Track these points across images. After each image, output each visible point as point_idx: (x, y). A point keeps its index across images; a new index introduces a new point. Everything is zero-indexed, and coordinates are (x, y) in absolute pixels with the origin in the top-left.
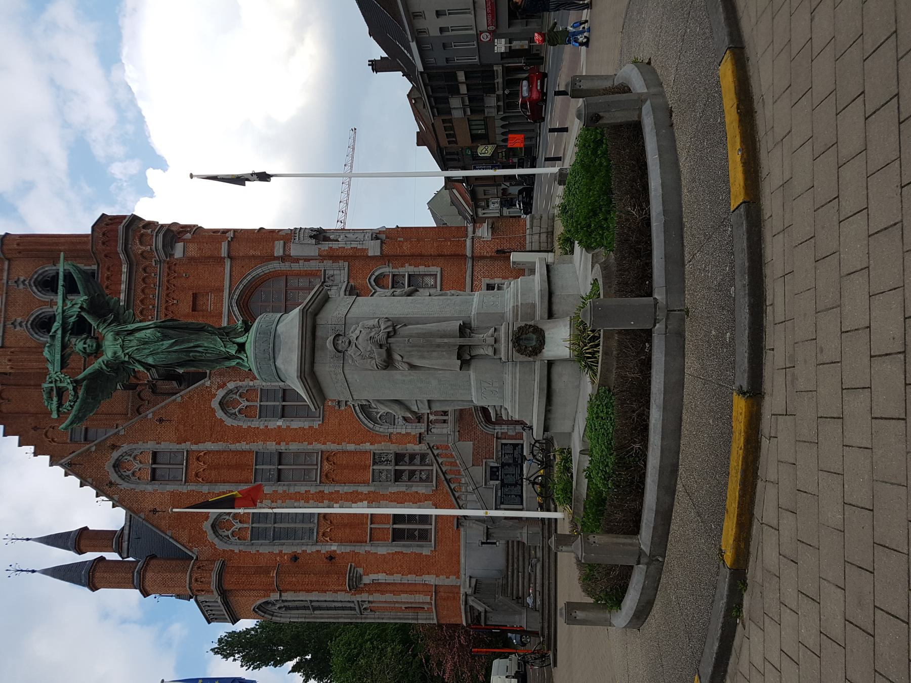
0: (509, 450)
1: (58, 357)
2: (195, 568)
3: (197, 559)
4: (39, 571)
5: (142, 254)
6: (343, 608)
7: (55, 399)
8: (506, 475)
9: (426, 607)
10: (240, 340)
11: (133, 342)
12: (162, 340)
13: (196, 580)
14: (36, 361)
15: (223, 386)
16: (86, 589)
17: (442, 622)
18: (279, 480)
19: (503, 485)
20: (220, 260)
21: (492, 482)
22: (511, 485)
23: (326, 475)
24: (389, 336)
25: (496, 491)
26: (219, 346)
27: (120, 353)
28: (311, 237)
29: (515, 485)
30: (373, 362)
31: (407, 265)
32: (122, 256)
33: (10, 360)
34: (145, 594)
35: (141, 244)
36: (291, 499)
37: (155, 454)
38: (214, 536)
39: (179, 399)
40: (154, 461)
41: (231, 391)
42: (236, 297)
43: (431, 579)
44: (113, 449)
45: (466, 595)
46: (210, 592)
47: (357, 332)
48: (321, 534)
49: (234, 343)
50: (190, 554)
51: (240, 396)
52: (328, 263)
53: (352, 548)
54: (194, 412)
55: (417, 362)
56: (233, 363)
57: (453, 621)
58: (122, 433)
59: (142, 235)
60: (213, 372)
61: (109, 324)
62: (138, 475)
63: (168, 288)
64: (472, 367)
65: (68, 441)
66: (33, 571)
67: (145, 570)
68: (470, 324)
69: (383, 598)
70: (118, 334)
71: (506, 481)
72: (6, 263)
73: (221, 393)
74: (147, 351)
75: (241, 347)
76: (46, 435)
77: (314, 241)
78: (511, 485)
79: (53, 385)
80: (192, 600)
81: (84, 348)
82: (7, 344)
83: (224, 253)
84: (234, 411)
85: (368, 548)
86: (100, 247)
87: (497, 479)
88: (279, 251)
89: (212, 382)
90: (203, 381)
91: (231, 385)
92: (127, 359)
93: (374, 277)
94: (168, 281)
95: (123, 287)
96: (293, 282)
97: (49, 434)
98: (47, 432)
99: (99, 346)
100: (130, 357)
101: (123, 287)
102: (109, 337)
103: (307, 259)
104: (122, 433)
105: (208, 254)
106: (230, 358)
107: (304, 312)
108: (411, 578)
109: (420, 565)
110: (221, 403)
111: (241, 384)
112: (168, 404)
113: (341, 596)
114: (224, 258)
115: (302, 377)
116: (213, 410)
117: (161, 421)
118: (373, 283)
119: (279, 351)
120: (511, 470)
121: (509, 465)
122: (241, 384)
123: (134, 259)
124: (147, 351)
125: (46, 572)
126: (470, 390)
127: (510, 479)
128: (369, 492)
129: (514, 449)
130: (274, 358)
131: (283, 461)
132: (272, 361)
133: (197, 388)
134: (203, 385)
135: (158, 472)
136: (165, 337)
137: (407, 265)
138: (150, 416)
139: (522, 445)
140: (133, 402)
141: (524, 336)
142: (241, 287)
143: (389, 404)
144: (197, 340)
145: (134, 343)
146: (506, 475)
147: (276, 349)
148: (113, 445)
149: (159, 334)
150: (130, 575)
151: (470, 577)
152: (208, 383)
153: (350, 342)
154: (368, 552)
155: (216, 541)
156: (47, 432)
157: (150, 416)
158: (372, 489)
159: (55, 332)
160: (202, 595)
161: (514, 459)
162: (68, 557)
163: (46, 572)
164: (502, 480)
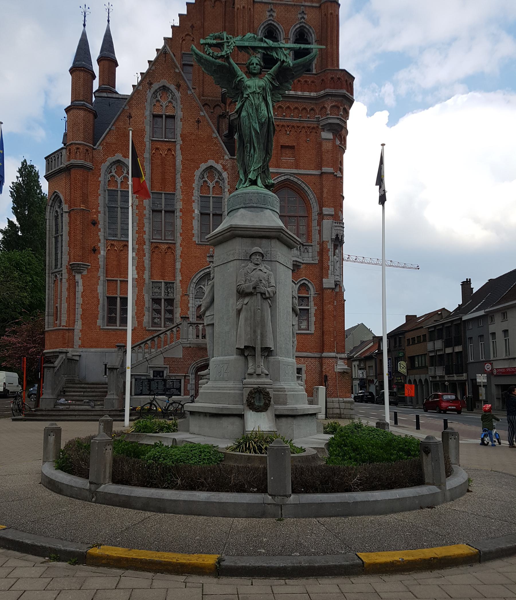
0: (176, 385)
1: (246, 44)
2: (87, 148)
3: (94, 149)
5: (324, 107)
6: (56, 260)
7: (215, 42)
8: (157, 383)
10: (259, 181)
11: (257, 100)
12: (259, 123)
13: (78, 148)
16: (71, 65)
17: (46, 335)
19: (150, 380)
20: (319, 166)
22: (150, 387)
23: (157, 247)
24: (262, 294)
25: (145, 375)
27: (249, 91)
28: (337, 235)
29: (150, 390)
32: (322, 92)
35: (332, 107)
37: (173, 117)
40: (167, 117)
41: (220, 174)
42: (292, 178)
43: (78, 326)
44: (177, 85)
45: (67, 353)
46: (69, 158)
47: (265, 270)
49: (257, 177)
50: (98, 144)
51: (217, 182)
52: (317, 248)
53: (102, 267)
54: (204, 147)
55: (242, 315)
57: (47, 342)
58: (189, 92)
60: (235, 161)
62: (157, 104)
63: (298, 127)
64: (239, 357)
65: (183, 52)
66: (84, 25)
67: (85, 110)
70: (264, 89)
72: (317, 5)
73: (219, 167)
75: (254, 183)
77: (334, 237)
78: (150, 387)
79: (225, 40)
80: (63, 145)
81: (253, 64)
82: (256, 5)
83: (325, 169)
84: (205, 177)
85: (102, 278)
86: (330, 76)
87: (154, 376)
88: (326, 211)
89: (227, 160)
90: (228, 153)
91: (225, 175)
92: (245, 96)
93: (307, 283)
94: (304, 127)
95: (300, 93)
97: (188, 38)
98: (190, 35)
99: (255, 75)
100: (247, 98)
101: (300, 93)
102: (262, 83)
103: (320, 232)
104: (189, 92)
109: (89, 318)
110: (211, 167)
111: (226, 182)
112: (211, 127)
114: (321, 170)
115: (232, 228)
117: (198, 122)
118: (302, 282)
119: (251, 211)
120: (161, 387)
121: (165, 385)
122: (226, 182)
123: (322, 100)
124: (251, 111)
125: (84, 35)
126: (222, 355)
127: (154, 385)
128: (144, 279)
129: (177, 389)
132: (244, 206)
133: (223, 149)
134: (226, 153)
135: (159, 120)
136: (261, 125)
139: (180, 395)
140: (212, 100)
141: (262, 396)
142: (299, 182)
143: (211, 294)
145: (257, 102)
146: (157, 383)
147: (252, 209)
148: (180, 85)
149: (263, 120)
150: (81, 98)
151: (80, 356)
152: (226, 157)
153: (257, 265)
155: (107, 164)
156: (190, 35)
158: (147, 281)
159: (265, 42)
160: (66, 153)
161: (170, 389)
163: (84, 35)
164: (153, 380)
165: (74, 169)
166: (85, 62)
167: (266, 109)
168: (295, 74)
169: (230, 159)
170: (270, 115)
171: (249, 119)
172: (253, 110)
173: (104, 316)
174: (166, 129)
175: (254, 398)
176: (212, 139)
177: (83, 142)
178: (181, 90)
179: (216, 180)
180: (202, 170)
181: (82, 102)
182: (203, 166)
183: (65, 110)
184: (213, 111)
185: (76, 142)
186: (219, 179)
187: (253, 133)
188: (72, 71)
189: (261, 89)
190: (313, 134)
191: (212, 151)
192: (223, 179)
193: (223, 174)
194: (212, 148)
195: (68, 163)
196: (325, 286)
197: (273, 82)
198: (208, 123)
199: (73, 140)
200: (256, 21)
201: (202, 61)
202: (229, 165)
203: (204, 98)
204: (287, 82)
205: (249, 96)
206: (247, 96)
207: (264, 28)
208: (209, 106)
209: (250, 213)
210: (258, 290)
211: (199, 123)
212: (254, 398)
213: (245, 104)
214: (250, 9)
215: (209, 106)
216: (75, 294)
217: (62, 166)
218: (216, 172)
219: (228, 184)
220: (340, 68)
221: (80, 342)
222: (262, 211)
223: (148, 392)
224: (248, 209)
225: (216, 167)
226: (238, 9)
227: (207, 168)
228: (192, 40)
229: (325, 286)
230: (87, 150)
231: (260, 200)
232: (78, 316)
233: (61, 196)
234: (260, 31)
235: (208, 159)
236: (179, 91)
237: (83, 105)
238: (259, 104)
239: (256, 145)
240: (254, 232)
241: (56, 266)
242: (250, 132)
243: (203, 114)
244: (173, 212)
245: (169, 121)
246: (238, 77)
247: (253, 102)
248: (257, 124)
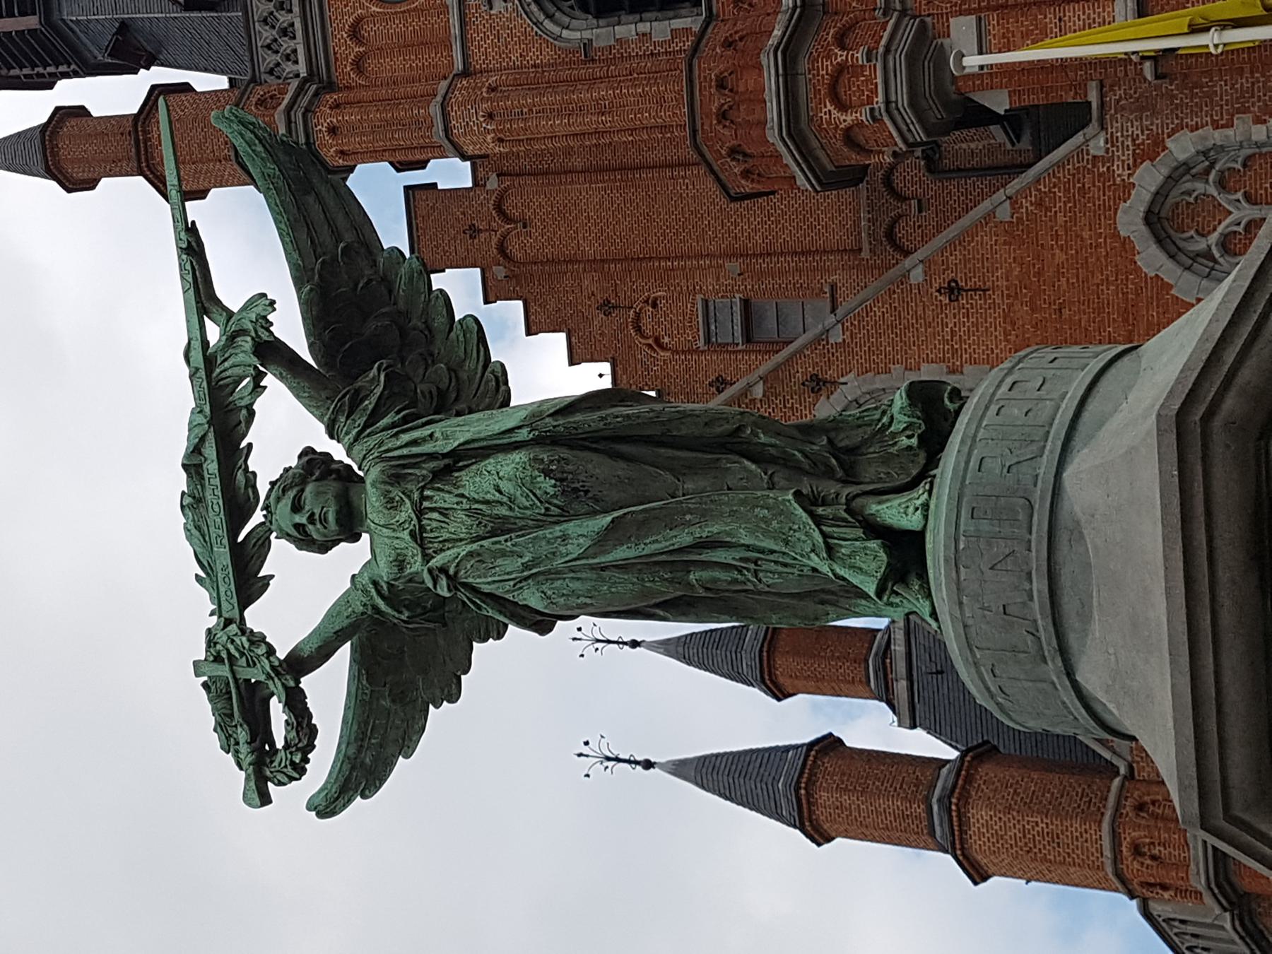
2: (1128, 808)
4: (663, 766)
12: (566, 515)
13: (1137, 850)
14: (560, 114)
15: (1151, 150)
27: (416, 565)
33: (490, 116)
34: (977, 874)
39: (1004, 213)
41: (1184, 168)
44: (816, 391)
49: (875, 529)
50: (1107, 755)
51: (1222, 184)
54: (1060, 256)
58: (837, 337)
60: (1111, 98)
65: (701, 344)
66: (648, 765)
67: (965, 798)
73: (1148, 179)
76: (638, 329)
82: (478, 62)
84: (1201, 245)
89: (1111, 141)
90: (1078, 139)
91: (1182, 147)
97: (647, 324)
98: (638, 316)
100: (453, 580)
104: (837, 337)
110: (1151, 218)
111: (1217, 136)
112: (970, 233)
116: (1126, 244)
117: (953, 290)
119: (1085, 617)
122: (1217, 136)
124: (511, 565)
125: (680, 769)
130: (1063, 651)
132: (1053, 668)
133: (1060, 165)
134: (1081, 151)
136: (574, 499)
138: (917, 276)
140: (871, 208)
144: (705, 516)
145: (460, 524)
147: (1069, 604)
148: (815, 378)
149: (547, 485)
150: (920, 810)
152: (1098, 146)
156: (638, 316)
157: (917, 276)
160: (1162, 900)
163: (680, 769)
165: (1235, 879)
166: (775, 780)
168: (349, 237)
169: (1103, 127)
170: (524, 435)
172: (503, 554)
176: (1020, 219)
177: (1106, 826)
178: (831, 374)
179: (1212, 191)
180: (1169, 264)
181: (935, 808)
182: (1151, 259)
183: (976, 883)
184: (914, 203)
185: (1107, 852)
186: (1207, 172)
187: (621, 553)
189: (396, 493)
191: (1074, 220)
192: (1205, 153)
193: (1182, 157)
194: (1061, 219)
195: (1208, 899)
197: (369, 404)
198: (951, 242)
199: (1101, 868)
200: (532, 57)
202: (1129, 129)
203: (866, 246)
205: (443, 570)
206: (443, 582)
207: (550, 17)
208: (895, 221)
209: (1096, 627)
211: (960, 289)
213: (486, 589)
214: (492, 89)
215: (895, 221)
217: (1228, 926)
218: (1174, 193)
219: (1230, 125)
222: (1077, 534)
224: (1072, 639)
225: (1147, 197)
226: (501, 140)
227: (1159, 242)
228: (654, 305)
230: (1140, 807)
231: (1002, 548)
234: (565, 33)
235: (1116, 235)
236: (835, 383)
237: (945, 802)
238: (470, 513)
239: (685, 539)
240: (1227, 639)
242: (622, 567)
243: (920, 269)
246: (376, 608)
247: (464, 550)
248: (572, 527)
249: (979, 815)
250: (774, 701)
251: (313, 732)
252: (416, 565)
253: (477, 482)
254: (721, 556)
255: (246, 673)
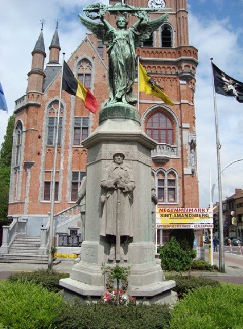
1: (115, 9)
3: (42, 95)
6: (17, 160)
7: (93, 9)
9: (16, 198)
10: (124, 99)
11: (122, 44)
12: (124, 58)
13: (33, 95)
16: (33, 50)
17: (9, 206)
18: (75, 128)
19: (68, 237)
20: (179, 99)
21: (69, 231)
22: (68, 241)
23: (77, 150)
24: (122, 189)
26: (120, 88)
28: (192, 140)
29: (68, 243)
30: (106, 179)
31: (180, 187)
34: (29, 74)
35: (185, 66)
36: (66, 134)
37: (89, 75)
38: (52, 101)
40: (86, 75)
42: (162, 106)
43: (27, 201)
45: (18, 218)
46: (27, 101)
47: (126, 168)
48: (49, 148)
52: (180, 149)
53: (42, 163)
56: (111, 96)
57: (9, 210)
59: (189, 67)
61: (133, 33)
62: (81, 68)
68: (131, 242)
69: (20, 178)
70: (128, 36)
71: (70, 238)
72: (175, 13)
74: (117, 51)
75: (120, 100)
77: (190, 142)
78: (68, 241)
79: (101, 7)
80: (26, 94)
81: (120, 21)
83: (183, 101)
85: (42, 170)
87: (71, 234)
88: (184, 125)
92: (114, 41)
93: (173, 171)
96: (170, 132)
99: (121, 28)
100: (115, 43)
102: (126, 32)
103: (182, 138)
105: (182, 94)
106: (114, 95)
107: (140, 135)
108: (28, 191)
109: (33, 197)
113: (22, 159)
114: (180, 101)
118: (170, 170)
120: (75, 241)
121: (78, 240)
124: (117, 51)
125: (41, 34)
128: (67, 170)
131: (84, 130)
135: (82, 77)
137: (180, 187)
143: (84, 188)
149: (127, 57)
151: (27, 220)
153: (119, 164)
154: (40, 170)
155: (50, 102)
158: (69, 171)
159: (129, 7)
162: (47, 44)
163: (41, 34)
164: (70, 236)
167: (129, 49)
171: (116, 56)
173: (42, 194)
174: (85, 81)
175: (113, 282)
188: (33, 53)
190: (175, 81)
196: (185, 173)
197: (135, 32)
201: (86, 23)
204: (146, 33)
210: (119, 186)
212: (113, 282)
216: (26, 180)
220: (190, 44)
221: (27, 211)
223: (67, 245)
229: (185, 173)
232: (27, 195)
233: (22, 122)
241: (17, 164)
244: (87, 128)
245: (88, 77)
249: (37, 75)
250: (49, 47)
251: (93, 19)
252: (117, 38)
253: (127, 47)
254: (119, 78)
255: (101, 10)
